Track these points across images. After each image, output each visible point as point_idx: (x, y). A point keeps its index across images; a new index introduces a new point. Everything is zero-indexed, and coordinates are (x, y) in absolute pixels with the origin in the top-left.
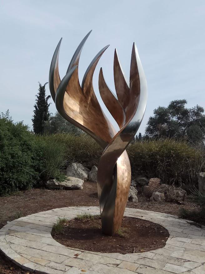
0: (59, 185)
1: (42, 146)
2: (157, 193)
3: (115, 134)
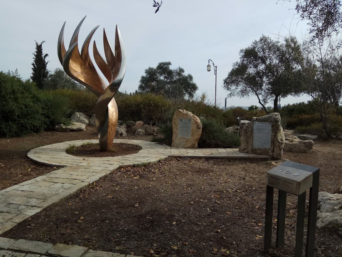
0: (66, 128)
2: (140, 130)
3: (106, 87)
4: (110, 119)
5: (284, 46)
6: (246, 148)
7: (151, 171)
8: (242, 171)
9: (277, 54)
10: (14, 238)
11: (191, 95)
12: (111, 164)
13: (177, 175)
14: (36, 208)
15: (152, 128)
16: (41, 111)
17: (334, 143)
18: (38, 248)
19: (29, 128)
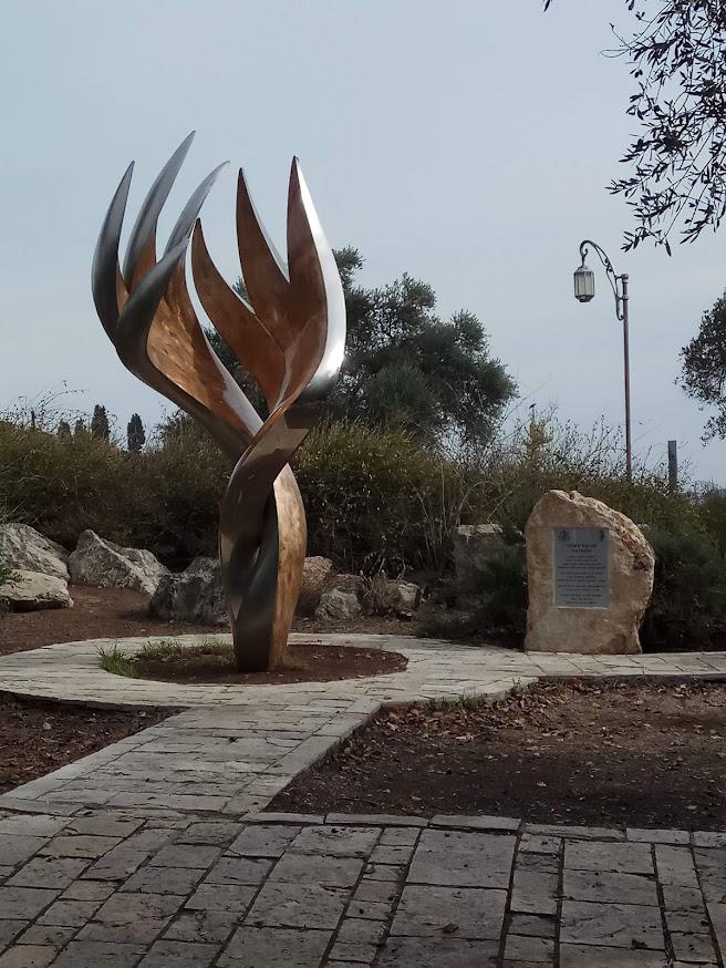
2: (336, 594)
11: (478, 430)
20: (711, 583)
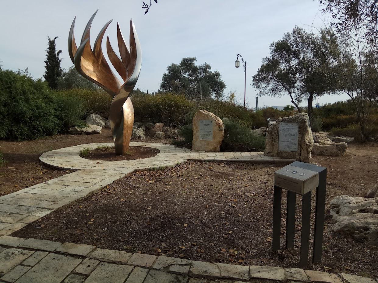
0: (81, 131)
1: (63, 99)
2: (159, 132)
4: (126, 120)
5: (319, 38)
6: (271, 151)
7: (168, 175)
8: (265, 175)
9: (312, 48)
10: (24, 238)
11: (218, 94)
12: (127, 167)
13: (195, 179)
14: (46, 210)
15: (172, 130)
16: (53, 112)
17: (372, 146)
18: (47, 246)
19: (41, 130)
20: (239, 134)
